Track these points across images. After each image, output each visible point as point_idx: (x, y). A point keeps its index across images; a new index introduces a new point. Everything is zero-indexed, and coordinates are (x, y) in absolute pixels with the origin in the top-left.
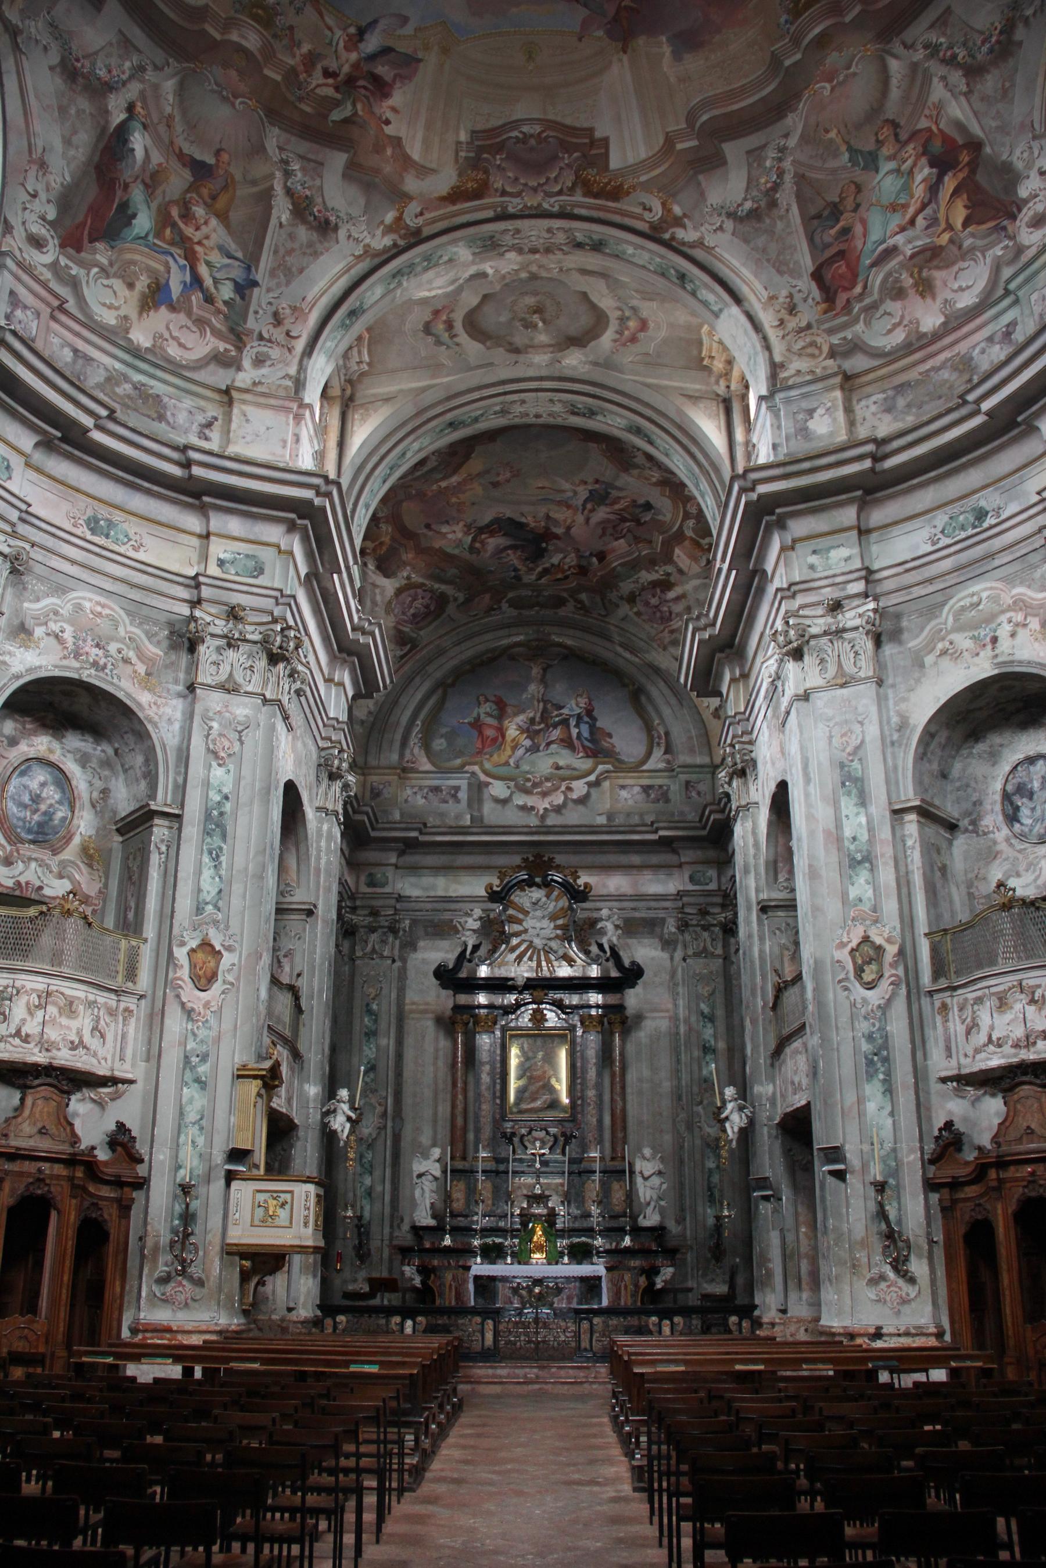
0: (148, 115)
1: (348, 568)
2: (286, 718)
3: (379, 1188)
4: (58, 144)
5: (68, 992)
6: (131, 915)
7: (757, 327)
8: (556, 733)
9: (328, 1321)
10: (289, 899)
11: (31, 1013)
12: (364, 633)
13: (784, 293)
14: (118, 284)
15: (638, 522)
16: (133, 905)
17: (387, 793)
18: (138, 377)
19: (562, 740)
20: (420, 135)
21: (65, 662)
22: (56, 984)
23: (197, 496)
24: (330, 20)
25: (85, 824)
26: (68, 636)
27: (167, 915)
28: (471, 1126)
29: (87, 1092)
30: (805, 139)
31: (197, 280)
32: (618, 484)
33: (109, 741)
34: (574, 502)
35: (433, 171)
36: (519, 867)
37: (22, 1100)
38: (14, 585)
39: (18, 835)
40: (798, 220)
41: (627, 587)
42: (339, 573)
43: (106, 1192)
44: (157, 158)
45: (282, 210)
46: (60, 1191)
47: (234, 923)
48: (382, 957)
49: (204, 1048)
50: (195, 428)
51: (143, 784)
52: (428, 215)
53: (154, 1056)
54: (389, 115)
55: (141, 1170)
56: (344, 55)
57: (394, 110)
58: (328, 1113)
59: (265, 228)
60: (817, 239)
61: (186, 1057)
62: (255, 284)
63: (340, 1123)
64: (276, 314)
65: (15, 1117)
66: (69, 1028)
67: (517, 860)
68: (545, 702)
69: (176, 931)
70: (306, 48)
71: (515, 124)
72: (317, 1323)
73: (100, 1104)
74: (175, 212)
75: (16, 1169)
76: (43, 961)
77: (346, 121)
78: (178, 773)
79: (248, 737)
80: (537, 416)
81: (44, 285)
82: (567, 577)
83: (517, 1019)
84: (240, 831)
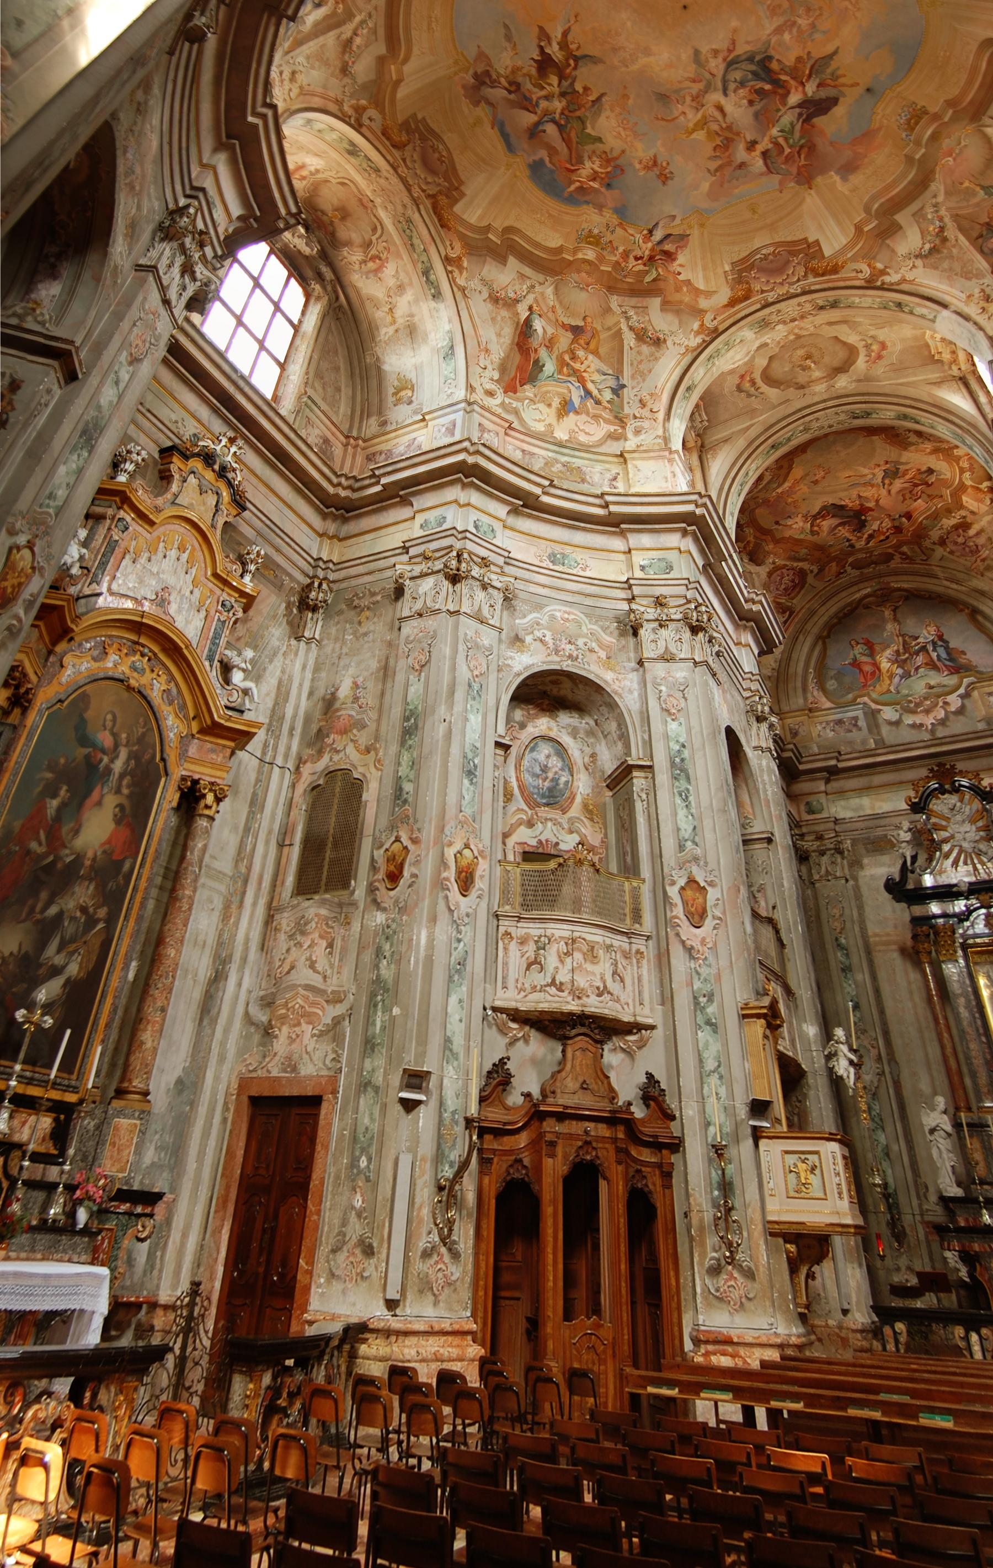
0: (541, 309)
1: (731, 556)
2: (714, 675)
3: (895, 1147)
4: (494, 338)
5: (589, 937)
6: (629, 859)
7: (967, 318)
8: (920, 659)
9: (887, 1330)
10: (750, 830)
11: (562, 962)
12: (754, 602)
13: (977, 291)
14: (541, 406)
15: (928, 485)
16: (629, 849)
17: (802, 731)
18: (564, 459)
19: (927, 664)
20: (701, 275)
21: (549, 658)
22: (581, 931)
23: (617, 525)
24: (631, 231)
25: (583, 785)
26: (548, 639)
27: (657, 856)
28: (965, 1069)
29: (617, 1041)
30: (948, 194)
31: (588, 393)
32: (903, 460)
33: (590, 715)
34: (875, 482)
35: (715, 292)
36: (927, 777)
37: (564, 1051)
38: (508, 609)
39: (535, 800)
40: (967, 243)
41: (935, 534)
42: (726, 560)
43: (646, 1155)
44: (550, 331)
45: (629, 339)
46: (606, 1156)
47: (711, 857)
48: (836, 878)
49: (708, 988)
50: (606, 482)
51: (620, 744)
52: (719, 318)
53: (667, 999)
54: (679, 269)
55: (674, 1127)
56: (644, 246)
57: (681, 265)
58: (829, 1057)
59: (622, 352)
60: (986, 250)
61: (695, 998)
62: (624, 386)
63: (842, 1067)
64: (641, 401)
65: (559, 1072)
66: (593, 974)
67: (924, 772)
68: (903, 636)
69: (666, 870)
70: (621, 249)
71: (757, 251)
72: (876, 1332)
73: (629, 1053)
74: (567, 358)
75: (566, 1131)
76: (566, 909)
77: (654, 280)
78: (644, 732)
79: (689, 693)
80: (830, 426)
81: (499, 417)
82: (888, 537)
83: (972, 925)
84: (700, 772)
